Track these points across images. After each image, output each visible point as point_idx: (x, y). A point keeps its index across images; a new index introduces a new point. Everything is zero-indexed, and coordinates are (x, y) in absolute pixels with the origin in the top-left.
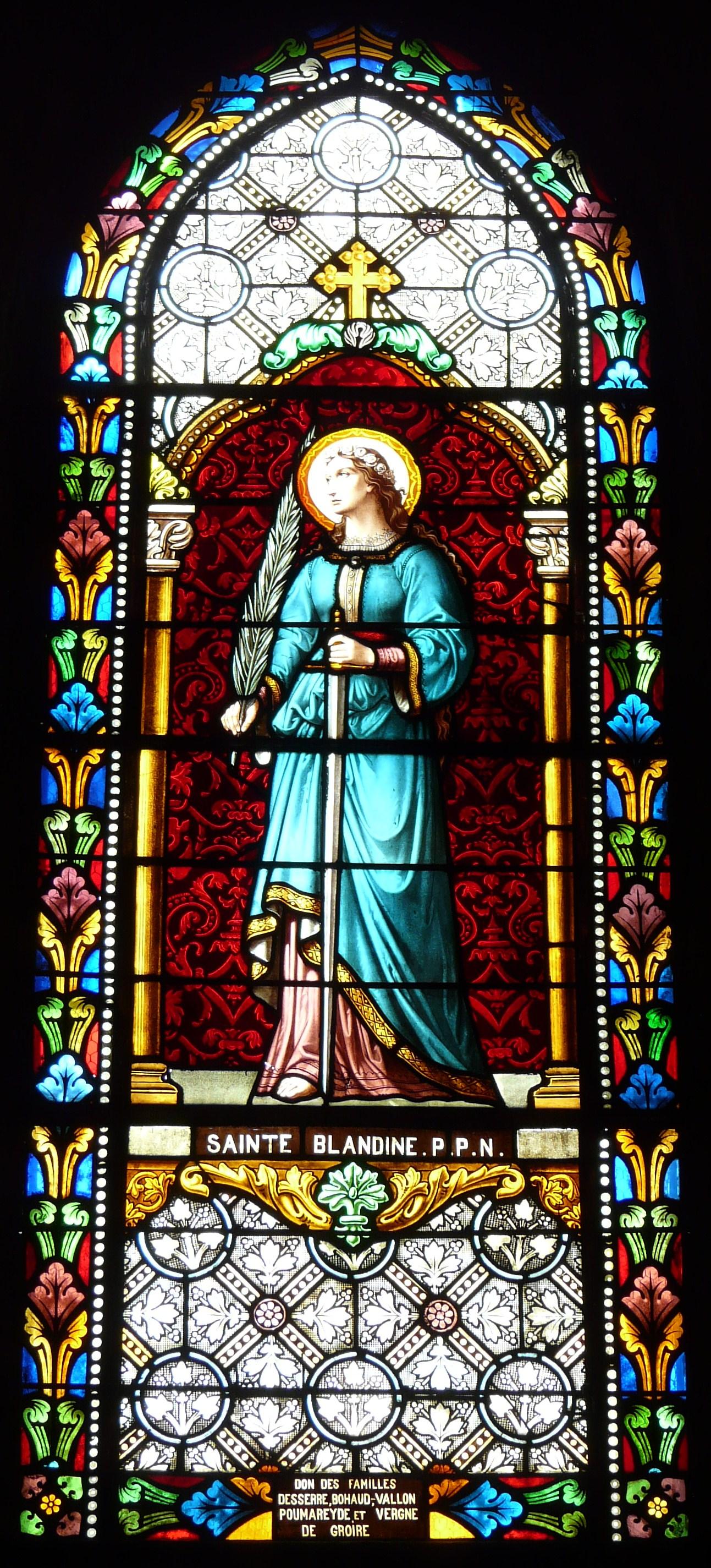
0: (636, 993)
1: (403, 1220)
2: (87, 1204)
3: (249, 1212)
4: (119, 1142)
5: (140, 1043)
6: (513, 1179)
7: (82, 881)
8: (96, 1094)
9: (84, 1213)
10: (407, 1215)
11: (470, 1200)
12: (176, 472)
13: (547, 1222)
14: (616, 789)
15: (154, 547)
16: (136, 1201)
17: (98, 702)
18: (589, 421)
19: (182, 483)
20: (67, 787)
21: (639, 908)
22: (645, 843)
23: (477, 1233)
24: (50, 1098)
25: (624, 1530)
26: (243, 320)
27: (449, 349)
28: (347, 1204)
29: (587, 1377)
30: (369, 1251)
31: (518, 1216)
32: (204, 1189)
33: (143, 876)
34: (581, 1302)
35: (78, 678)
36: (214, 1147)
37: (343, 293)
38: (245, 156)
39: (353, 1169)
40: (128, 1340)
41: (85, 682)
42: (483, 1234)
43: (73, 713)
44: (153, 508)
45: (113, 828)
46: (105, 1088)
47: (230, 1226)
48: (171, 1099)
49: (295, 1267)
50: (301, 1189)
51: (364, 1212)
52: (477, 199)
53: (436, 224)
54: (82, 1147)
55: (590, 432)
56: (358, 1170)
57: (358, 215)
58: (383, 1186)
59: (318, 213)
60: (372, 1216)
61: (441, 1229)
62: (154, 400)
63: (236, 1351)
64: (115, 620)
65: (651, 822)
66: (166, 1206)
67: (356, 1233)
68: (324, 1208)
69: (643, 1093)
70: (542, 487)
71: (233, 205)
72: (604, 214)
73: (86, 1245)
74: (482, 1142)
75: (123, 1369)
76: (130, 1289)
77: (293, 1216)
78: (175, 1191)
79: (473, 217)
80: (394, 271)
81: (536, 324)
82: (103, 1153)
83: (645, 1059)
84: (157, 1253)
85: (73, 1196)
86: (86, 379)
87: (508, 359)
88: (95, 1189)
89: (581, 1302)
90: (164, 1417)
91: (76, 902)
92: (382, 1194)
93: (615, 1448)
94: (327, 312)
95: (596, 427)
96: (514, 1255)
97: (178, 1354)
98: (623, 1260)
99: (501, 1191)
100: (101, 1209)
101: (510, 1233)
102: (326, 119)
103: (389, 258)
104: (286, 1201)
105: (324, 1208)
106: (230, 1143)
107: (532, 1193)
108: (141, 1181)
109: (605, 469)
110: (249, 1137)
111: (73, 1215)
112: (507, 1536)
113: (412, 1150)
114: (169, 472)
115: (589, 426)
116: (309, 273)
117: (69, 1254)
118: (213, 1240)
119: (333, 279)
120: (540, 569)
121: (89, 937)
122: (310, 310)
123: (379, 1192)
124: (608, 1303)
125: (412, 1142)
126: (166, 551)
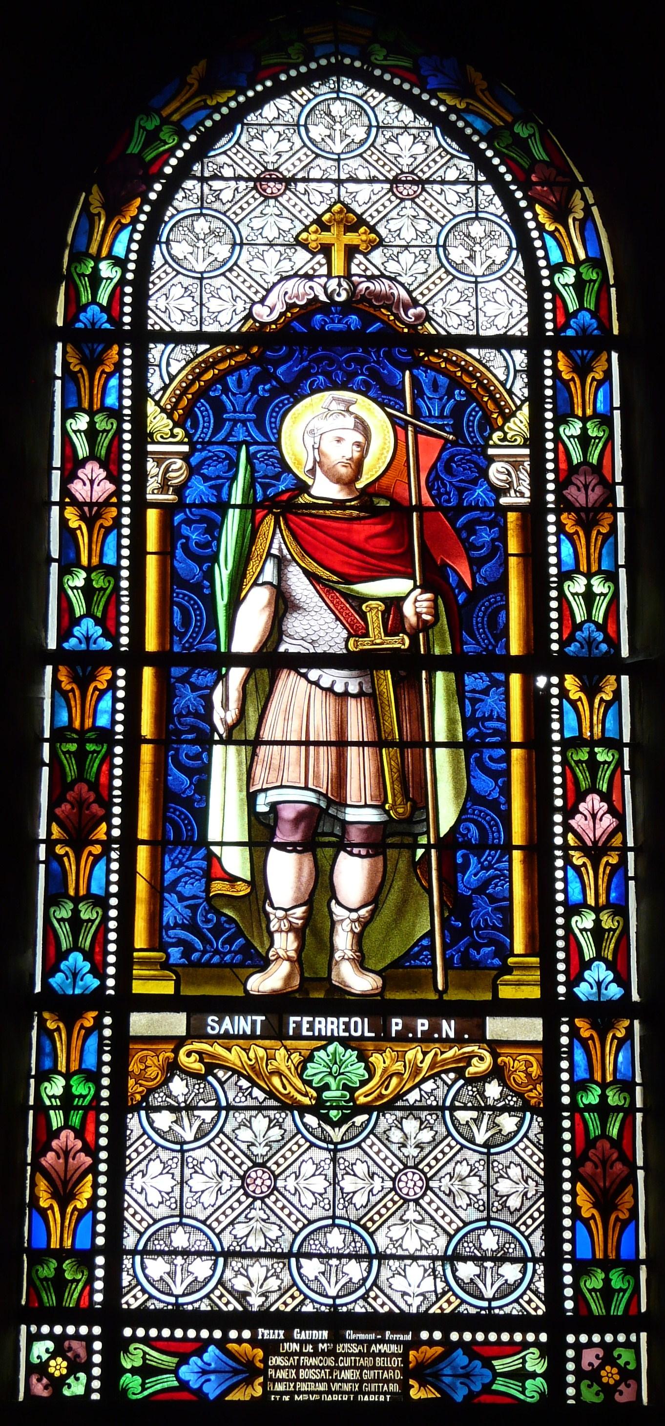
1: (381, 1096)
2: (93, 1077)
3: (241, 1087)
4: (121, 1025)
6: (482, 1059)
8: (103, 987)
10: (384, 1092)
11: (443, 1076)
13: (512, 1101)
14: (569, 545)
15: (152, 484)
16: (138, 1078)
18: (552, 529)
19: (176, 424)
22: (590, 432)
24: (60, 992)
27: (422, 302)
30: (350, 1123)
32: (199, 1067)
34: (542, 1173)
35: (76, 948)
36: (213, 1028)
38: (239, 127)
40: (129, 1206)
42: (453, 1108)
44: (151, 448)
45: (113, 913)
46: (111, 982)
47: (224, 1103)
49: (283, 1138)
51: (345, 1087)
52: (449, 287)
54: (89, 1023)
56: (341, 1049)
58: (363, 1064)
61: (417, 1104)
65: (608, 905)
66: (167, 1081)
67: (337, 1108)
68: (308, 1083)
69: (595, 989)
72: (559, 179)
75: (125, 1235)
76: (156, 323)
78: (173, 1068)
79: (443, 182)
80: (373, 229)
81: (500, 278)
84: (155, 1125)
92: (362, 1071)
93: (559, 775)
94: (312, 268)
95: (557, 534)
99: (471, 1070)
102: (311, 96)
103: (369, 219)
104: (276, 1081)
107: (497, 1072)
108: (142, 1060)
112: (476, 1401)
114: (164, 416)
119: (313, 237)
122: (296, 268)
123: (360, 1069)
124: (567, 1174)
126: (164, 487)
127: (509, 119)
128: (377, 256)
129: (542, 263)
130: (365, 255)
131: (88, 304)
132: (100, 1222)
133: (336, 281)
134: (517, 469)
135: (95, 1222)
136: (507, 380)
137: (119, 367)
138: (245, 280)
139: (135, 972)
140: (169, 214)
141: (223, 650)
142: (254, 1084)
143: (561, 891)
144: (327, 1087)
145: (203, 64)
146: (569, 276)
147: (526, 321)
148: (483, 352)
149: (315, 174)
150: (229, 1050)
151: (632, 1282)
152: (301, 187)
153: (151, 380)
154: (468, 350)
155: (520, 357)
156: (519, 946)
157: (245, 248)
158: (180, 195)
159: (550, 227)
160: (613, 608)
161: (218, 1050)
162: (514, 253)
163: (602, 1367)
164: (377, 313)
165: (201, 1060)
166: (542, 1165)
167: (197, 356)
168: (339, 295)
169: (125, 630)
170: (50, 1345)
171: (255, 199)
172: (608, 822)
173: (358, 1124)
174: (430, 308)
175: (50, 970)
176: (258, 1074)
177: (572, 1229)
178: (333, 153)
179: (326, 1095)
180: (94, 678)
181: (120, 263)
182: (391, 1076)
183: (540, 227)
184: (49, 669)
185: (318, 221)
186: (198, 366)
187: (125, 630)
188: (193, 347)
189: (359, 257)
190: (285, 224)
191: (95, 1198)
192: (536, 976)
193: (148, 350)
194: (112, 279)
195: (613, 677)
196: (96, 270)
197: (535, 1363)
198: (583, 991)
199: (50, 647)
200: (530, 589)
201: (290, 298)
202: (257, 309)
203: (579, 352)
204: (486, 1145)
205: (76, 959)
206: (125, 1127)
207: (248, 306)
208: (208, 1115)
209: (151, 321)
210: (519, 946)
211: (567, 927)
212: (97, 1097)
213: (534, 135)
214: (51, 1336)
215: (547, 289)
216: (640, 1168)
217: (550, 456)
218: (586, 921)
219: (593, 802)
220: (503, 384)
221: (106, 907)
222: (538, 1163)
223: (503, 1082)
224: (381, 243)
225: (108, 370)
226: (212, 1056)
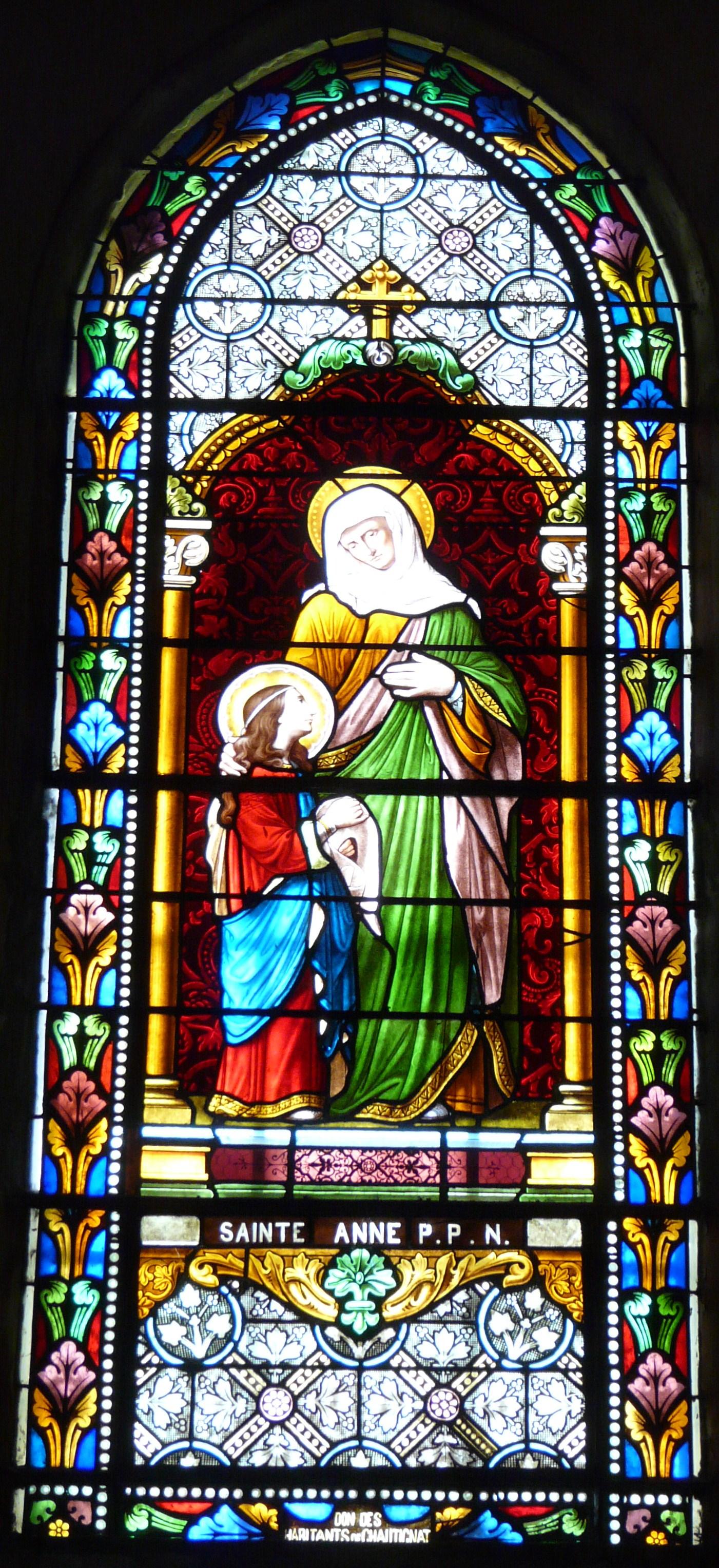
3: (258, 1299)
6: (522, 1266)
7: (92, 1086)
17: (89, 1364)
26: (236, 1448)
27: (470, 368)
28: (354, 1288)
32: (212, 1280)
34: (580, 1383)
36: (226, 1236)
41: (86, 1070)
43: (82, 917)
44: (170, 524)
50: (308, 1276)
51: (371, 1297)
55: (615, 990)
62: (170, 417)
64: (132, 639)
66: (174, 1293)
68: (331, 1292)
82: (115, 1229)
84: (197, 312)
86: (105, 395)
87: (531, 376)
90: (180, 1343)
95: (622, 985)
99: (508, 1278)
100: (131, 838)
106: (243, 1232)
110: (262, 1225)
120: (556, 586)
123: (386, 1276)
128: (423, 318)
130: (408, 316)
131: (95, 531)
133: (375, 344)
136: (562, 454)
139: (146, 1101)
140: (194, 270)
141: (148, 1082)
142: (272, 1296)
147: (586, 389)
148: (538, 422)
154: (522, 421)
155: (577, 429)
158: (207, 249)
164: (423, 379)
165: (215, 1273)
166: (586, 357)
167: (222, 425)
168: (379, 359)
170: (51, 1504)
172: (667, 742)
173: (384, 1340)
174: (479, 374)
175: (40, 1361)
181: (124, 650)
184: (73, 415)
185: (357, 279)
186: (222, 436)
188: (218, 416)
191: (133, 593)
195: (672, 425)
196: (111, 331)
199: (19, 1464)
201: (325, 363)
202: (290, 375)
205: (69, 1350)
206: (173, 319)
207: (279, 371)
209: (174, 390)
211: (621, 1313)
214: (52, 1496)
216: (685, 567)
218: (637, 503)
219: (652, 721)
220: (558, 457)
222: (582, 356)
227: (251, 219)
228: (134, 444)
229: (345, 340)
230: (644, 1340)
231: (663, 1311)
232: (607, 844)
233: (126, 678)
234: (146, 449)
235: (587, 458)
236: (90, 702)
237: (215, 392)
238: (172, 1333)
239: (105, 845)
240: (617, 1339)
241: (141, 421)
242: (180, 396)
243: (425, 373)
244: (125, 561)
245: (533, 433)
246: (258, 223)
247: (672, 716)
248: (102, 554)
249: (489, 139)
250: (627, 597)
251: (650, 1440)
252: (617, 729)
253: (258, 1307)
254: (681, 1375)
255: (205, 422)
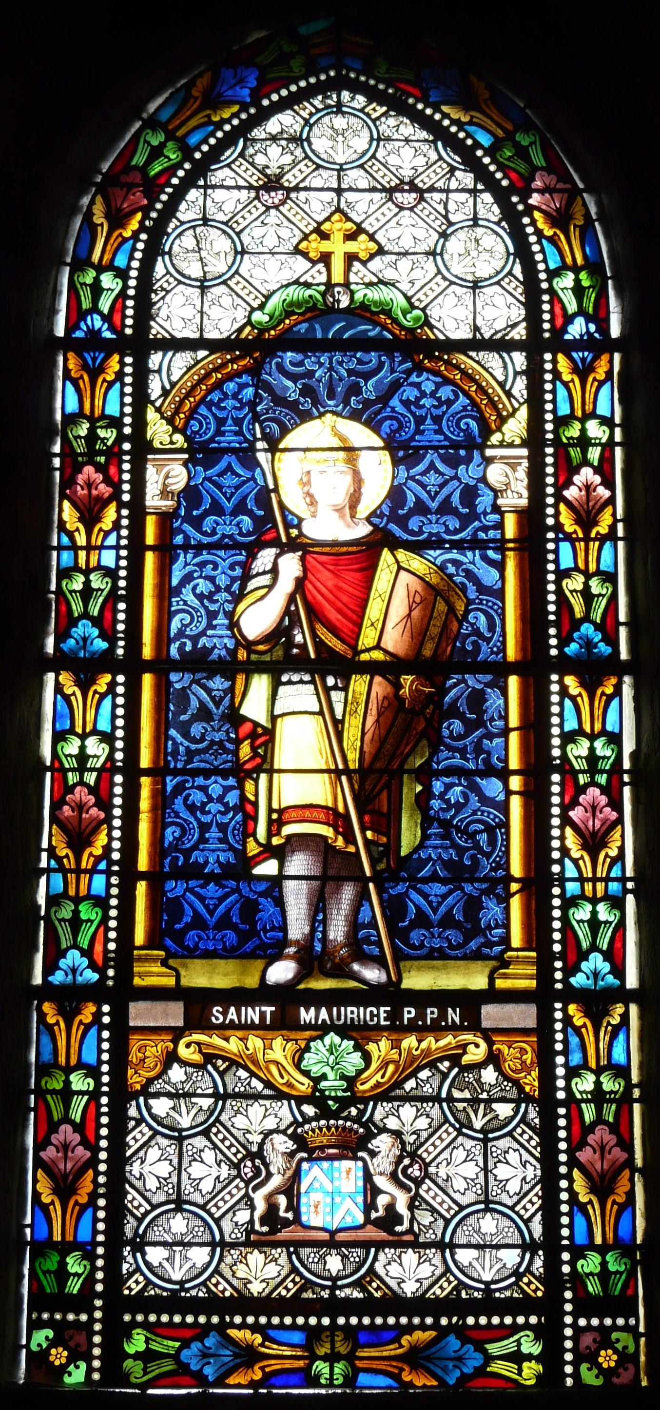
0: (589, 887)
2: (93, 1072)
3: (239, 1078)
5: (140, 937)
6: (477, 1046)
7: (77, 1138)
9: (90, 1081)
12: (170, 421)
20: (62, 1043)
21: (594, 807)
23: (444, 1100)
25: (576, 1375)
28: (327, 1070)
29: (543, 1228)
31: (483, 1231)
32: (197, 1058)
33: (141, 888)
34: (538, 1155)
37: (325, 258)
39: (332, 1038)
41: (72, 1123)
45: (113, 913)
48: (171, 982)
50: (285, 1057)
51: (343, 1077)
53: (409, 198)
56: (337, 1039)
57: (339, 191)
59: (306, 189)
60: (351, 1081)
63: (247, 169)
66: (164, 1072)
70: (505, 429)
71: (229, 182)
72: (560, 186)
73: (92, 1105)
74: (450, 1010)
76: (158, 333)
77: (279, 1081)
78: (171, 1058)
80: (372, 237)
83: (587, 618)
84: (153, 1111)
85: (81, 1065)
88: (114, 728)
89: (538, 1155)
91: (72, 1158)
93: (554, 636)
95: (564, 1031)
96: (483, 1268)
97: (172, 1206)
98: (558, 310)
101: (477, 1247)
104: (273, 1068)
105: (306, 1074)
107: (494, 1059)
109: (561, 422)
111: (79, 1082)
113: (385, 1019)
114: (164, 422)
115: (556, 783)
116: (295, 241)
117: (77, 1116)
118: (206, 1103)
119: (315, 246)
121: (107, 522)
123: (356, 1059)
124: (563, 1158)
125: (385, 1012)
126: (165, 493)
127: (509, 127)
128: (376, 264)
129: (541, 267)
132: (101, 1220)
134: (514, 470)
135: (97, 1173)
136: (506, 380)
137: (120, 375)
138: (247, 169)
139: (136, 969)
140: (172, 225)
142: (253, 1074)
143: (550, 392)
144: (324, 1077)
145: (180, 864)
146: (567, 281)
148: (481, 354)
149: (317, 183)
150: (227, 1040)
151: (618, 914)
152: (303, 195)
153: (151, 386)
155: (519, 359)
156: (516, 940)
157: (246, 256)
158: (183, 206)
159: (548, 232)
160: (612, 607)
161: (217, 1041)
162: (512, 257)
163: (599, 1366)
165: (200, 1051)
166: (539, 1149)
167: (198, 362)
169: (118, 801)
171: (235, 1155)
176: (255, 1062)
177: (570, 1214)
178: (334, 163)
179: (323, 1084)
180: (79, 1012)
182: (387, 1064)
183: (539, 233)
185: (318, 231)
187: (118, 801)
189: (357, 265)
190: (285, 233)
192: (532, 970)
193: (148, 356)
194: (113, 290)
196: (97, 280)
197: (530, 1346)
198: (578, 980)
200: (527, 567)
203: (581, 354)
204: (482, 1131)
208: (206, 1103)
209: (154, 332)
210: (516, 940)
211: (565, 919)
212: (115, 587)
213: (535, 142)
215: (545, 292)
217: (546, 317)
220: (502, 385)
221: (106, 907)
223: (498, 1069)
224: (381, 251)
225: (109, 378)
226: (208, 1045)
227: (201, 1151)
228: (118, 385)
229: (307, 285)
230: (572, 306)
231: (612, 1267)
232: (550, 693)
233: (120, 300)
234: (120, 701)
235: (528, 387)
236: (68, 949)
237: (192, 333)
238: (161, 1106)
239: (94, 747)
240: (552, 432)
241: (122, 364)
242: (159, 336)
243: (378, 313)
244: (88, 1154)
245: (478, 363)
246: (209, 1156)
247: (604, 469)
248: (89, 485)
249: (437, 109)
250: (572, 840)
251: (587, 858)
252: (561, 805)
253: (239, 1085)
254: (609, 483)
255: (181, 361)
